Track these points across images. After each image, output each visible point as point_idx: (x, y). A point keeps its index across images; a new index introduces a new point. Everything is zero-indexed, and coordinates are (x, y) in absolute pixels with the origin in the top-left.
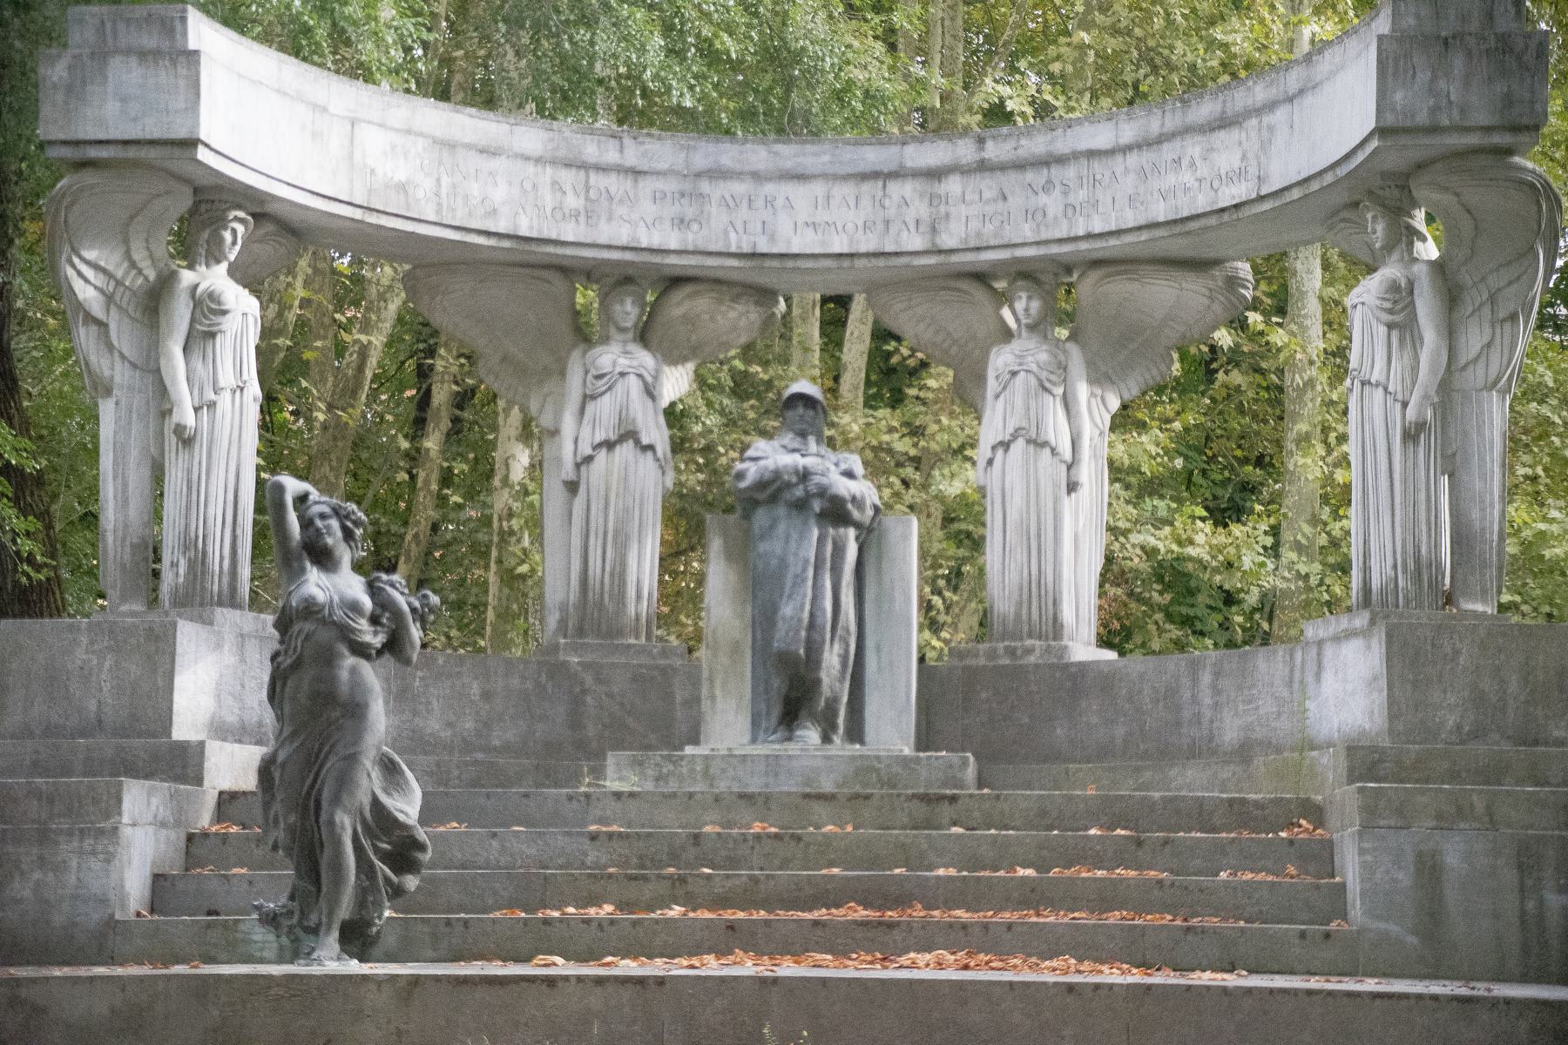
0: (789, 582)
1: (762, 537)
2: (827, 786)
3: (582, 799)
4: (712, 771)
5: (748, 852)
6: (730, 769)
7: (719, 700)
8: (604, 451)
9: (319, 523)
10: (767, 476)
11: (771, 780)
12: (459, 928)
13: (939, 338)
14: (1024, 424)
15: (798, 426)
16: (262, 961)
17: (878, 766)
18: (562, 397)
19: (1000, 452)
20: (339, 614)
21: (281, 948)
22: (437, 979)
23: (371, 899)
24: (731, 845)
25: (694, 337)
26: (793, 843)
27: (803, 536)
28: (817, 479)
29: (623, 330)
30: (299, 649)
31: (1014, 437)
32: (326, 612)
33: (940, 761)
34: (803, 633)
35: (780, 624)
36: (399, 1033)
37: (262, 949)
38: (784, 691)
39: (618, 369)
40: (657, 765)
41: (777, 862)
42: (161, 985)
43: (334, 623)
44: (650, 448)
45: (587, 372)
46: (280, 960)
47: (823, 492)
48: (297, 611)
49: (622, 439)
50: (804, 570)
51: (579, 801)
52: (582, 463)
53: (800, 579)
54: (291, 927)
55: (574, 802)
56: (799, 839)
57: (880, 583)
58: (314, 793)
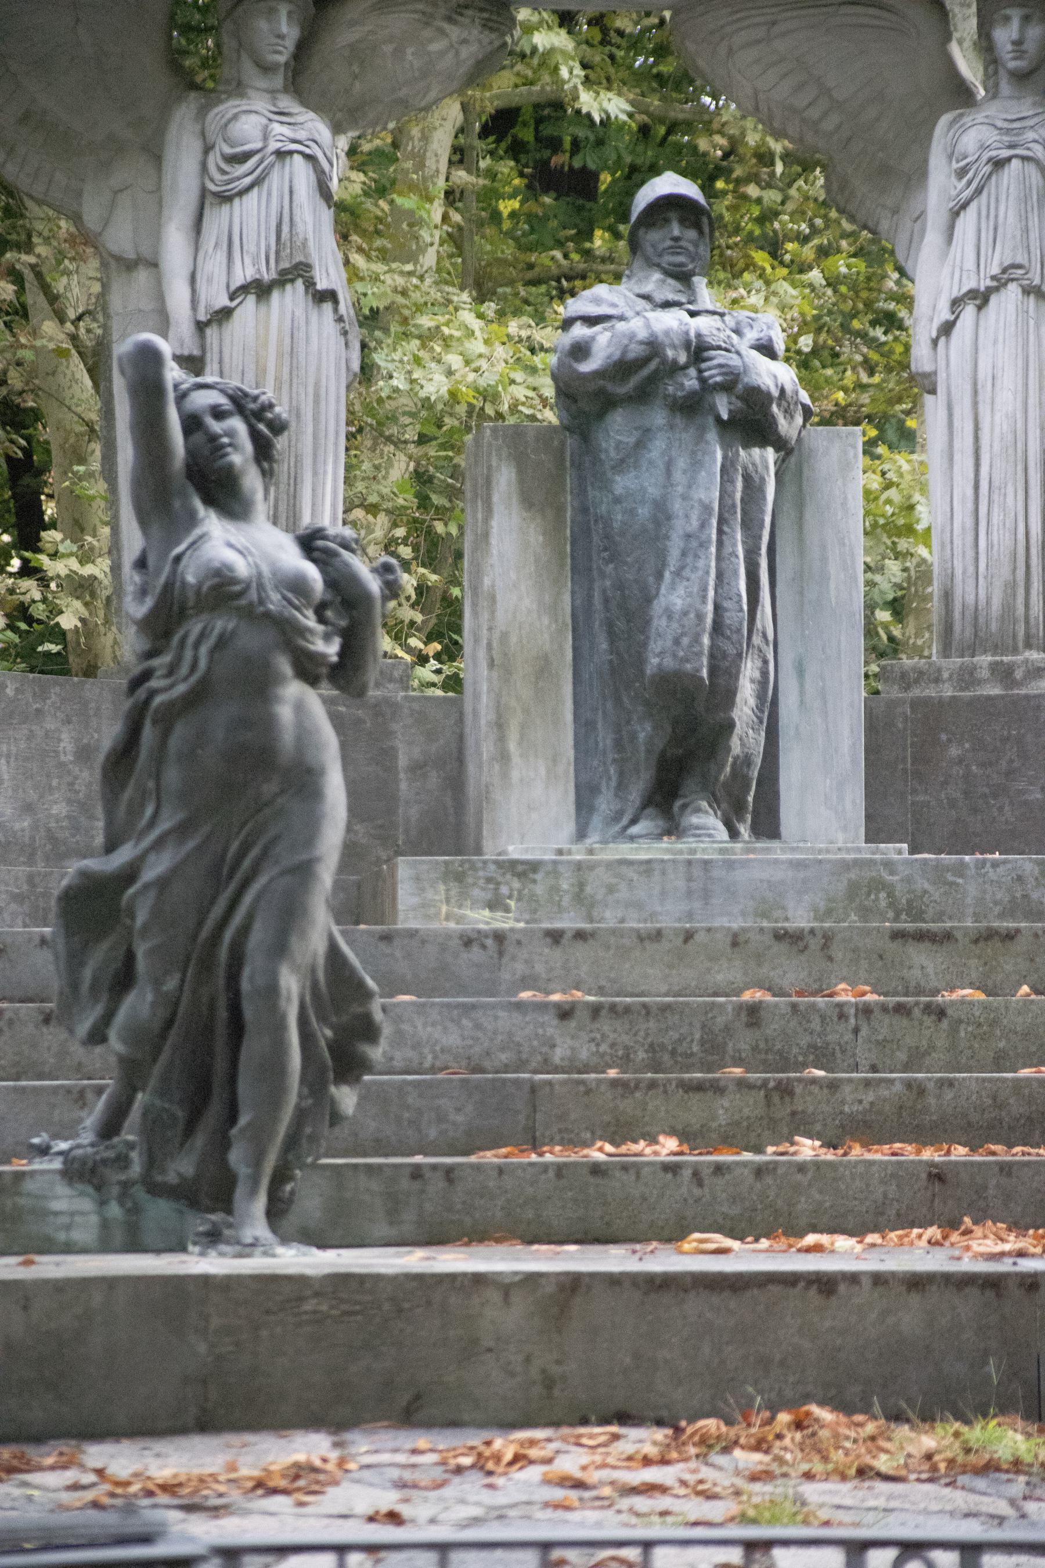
0: (675, 546)
1: (620, 466)
2: (800, 919)
3: (489, 942)
4: (588, 890)
5: (849, 1037)
6: (623, 886)
7: (516, 759)
8: (251, 299)
9: (216, 426)
10: (635, 351)
11: (697, 905)
12: (437, 1184)
13: (801, 101)
14: (1019, 259)
15: (668, 259)
16: (69, 1249)
17: (889, 878)
18: (157, 197)
19: (969, 311)
20: (275, 601)
21: (105, 1225)
22: (614, 1280)
23: (308, 1130)
24: (816, 1024)
25: (358, 86)
26: (928, 1021)
27: (696, 464)
28: (720, 358)
29: (266, 69)
30: (203, 663)
31: (1000, 283)
32: (253, 595)
33: (1001, 870)
34: (706, 640)
35: (659, 623)
36: (549, 1383)
37: (68, 1227)
38: (660, 744)
39: (273, 146)
40: (489, 880)
41: (902, 1056)
42: (97, 1299)
43: (267, 615)
44: (330, 296)
45: (207, 149)
46: (105, 1247)
47: (731, 383)
48: (198, 593)
49: (284, 279)
50: (704, 525)
51: (484, 947)
52: (208, 323)
53: (694, 542)
54: (126, 1185)
55: (476, 949)
56: (941, 1013)
57: (802, 550)
58: (228, 935)
